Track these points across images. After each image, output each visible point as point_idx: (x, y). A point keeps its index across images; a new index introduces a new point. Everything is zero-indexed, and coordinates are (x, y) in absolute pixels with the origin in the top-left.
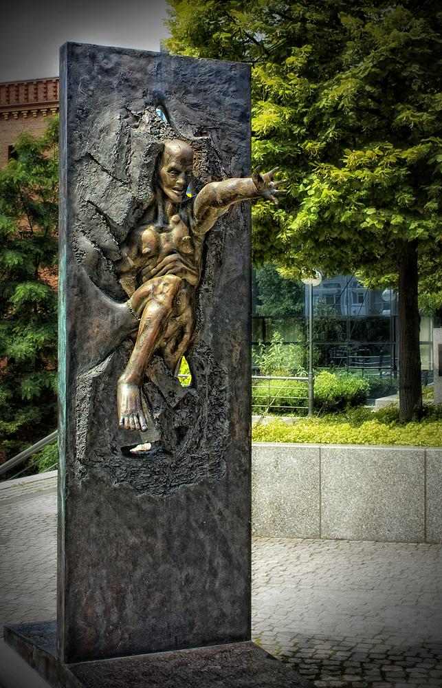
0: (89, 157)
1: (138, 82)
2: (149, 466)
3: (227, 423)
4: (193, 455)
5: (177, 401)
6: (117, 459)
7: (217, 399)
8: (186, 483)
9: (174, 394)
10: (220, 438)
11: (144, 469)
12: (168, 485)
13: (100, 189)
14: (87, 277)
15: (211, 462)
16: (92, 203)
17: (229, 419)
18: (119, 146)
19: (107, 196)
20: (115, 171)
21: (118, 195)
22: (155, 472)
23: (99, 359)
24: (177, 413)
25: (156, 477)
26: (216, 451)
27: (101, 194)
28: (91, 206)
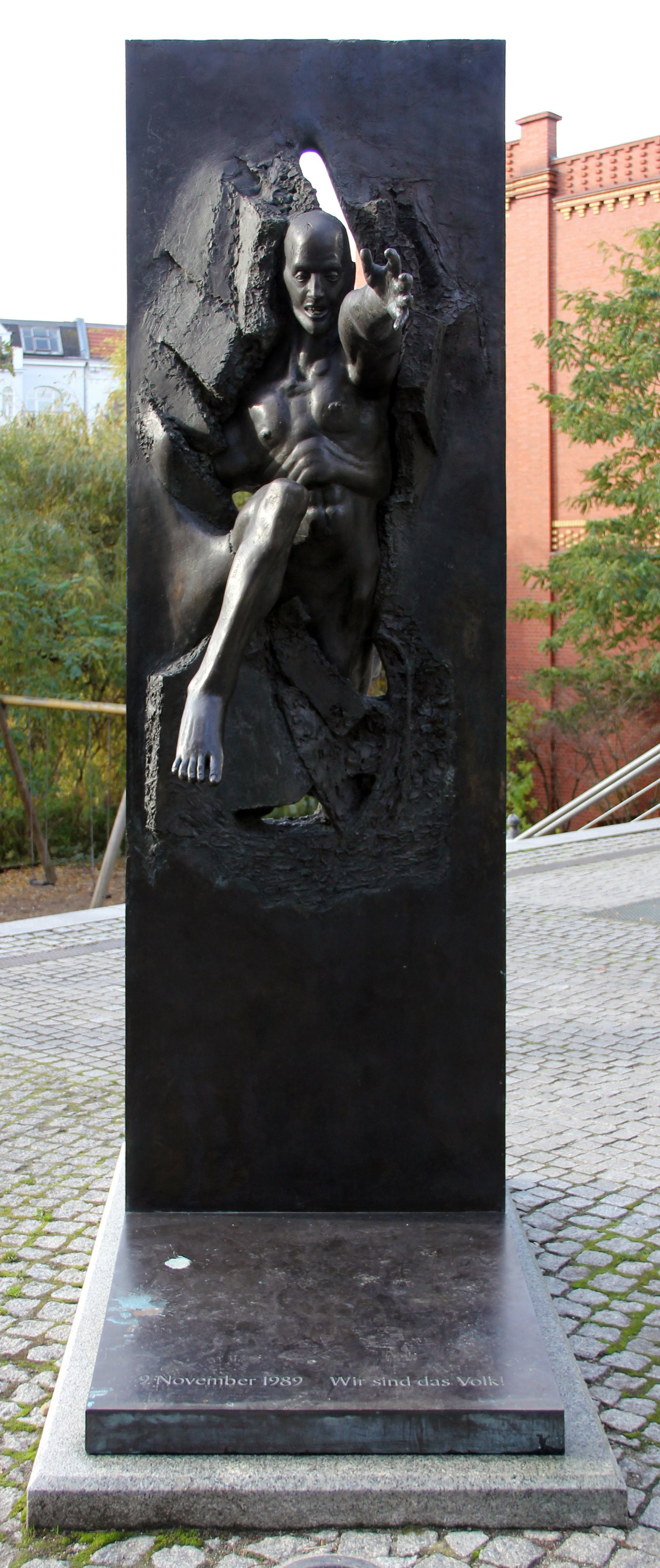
0: (167, 257)
1: (97, 734)
2: (292, 850)
3: (450, 774)
4: (381, 832)
5: (349, 724)
6: (225, 833)
7: (433, 722)
8: (367, 887)
9: (341, 710)
10: (438, 800)
11: (282, 855)
12: (330, 889)
13: (182, 321)
14: (361, 280)
15: (418, 848)
16: (170, 348)
17: (455, 763)
18: (217, 232)
19: (194, 329)
20: (210, 281)
21: (212, 329)
22: (303, 862)
23: (187, 642)
24: (353, 749)
25: (304, 871)
26: (429, 827)
27: (184, 329)
28: (167, 353)
